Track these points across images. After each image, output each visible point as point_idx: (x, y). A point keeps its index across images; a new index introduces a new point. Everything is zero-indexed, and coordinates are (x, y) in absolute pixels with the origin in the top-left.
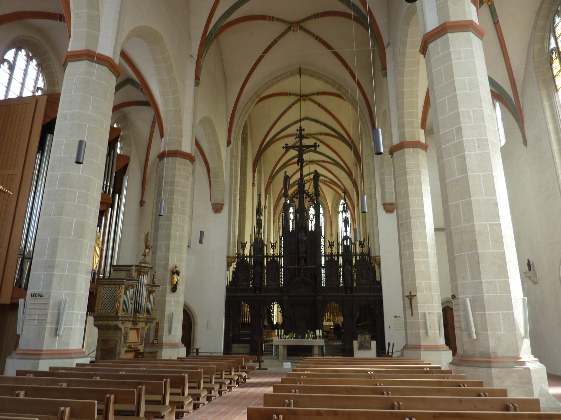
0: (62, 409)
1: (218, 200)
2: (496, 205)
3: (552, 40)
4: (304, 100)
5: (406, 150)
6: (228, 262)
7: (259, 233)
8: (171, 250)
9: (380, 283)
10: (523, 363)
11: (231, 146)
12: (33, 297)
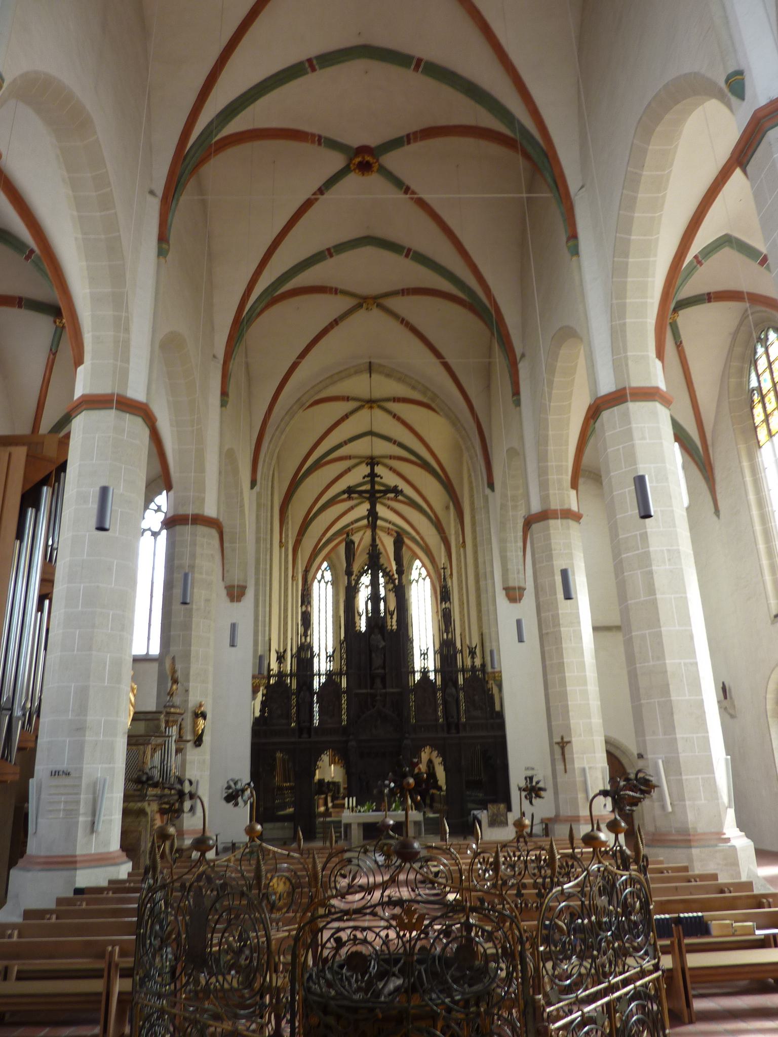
0: (110, 948)
1: (236, 578)
2: (691, 637)
3: (753, 376)
5: (552, 522)
6: (255, 685)
7: (305, 634)
8: (192, 678)
10: (728, 840)
11: (257, 488)
12: (55, 775)
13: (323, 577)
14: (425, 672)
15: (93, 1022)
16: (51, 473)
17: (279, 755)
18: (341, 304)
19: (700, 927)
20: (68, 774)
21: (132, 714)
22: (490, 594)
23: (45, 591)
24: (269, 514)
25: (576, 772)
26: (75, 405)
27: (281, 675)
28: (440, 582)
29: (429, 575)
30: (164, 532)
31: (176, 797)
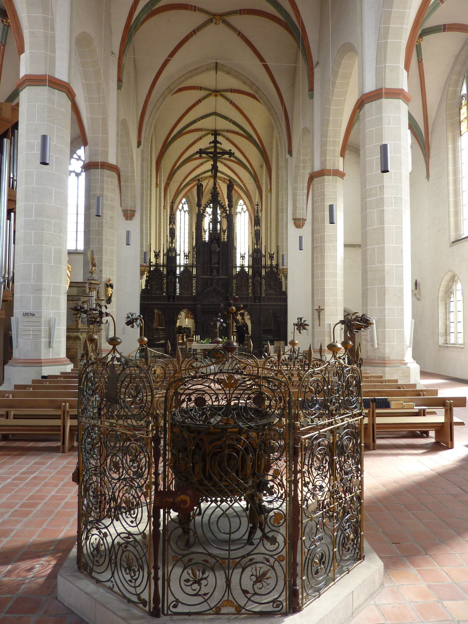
0: (64, 404)
4: (216, 96)
5: (326, 177)
7: (172, 242)
8: (103, 264)
9: (285, 294)
11: (141, 147)
13: (183, 207)
14: (242, 267)
15: (58, 440)
16: (9, 129)
17: (156, 311)
18: (199, 18)
19: (385, 404)
20: (34, 315)
21: (69, 282)
22: (284, 222)
23: (11, 207)
24: (149, 165)
25: (326, 326)
26: (21, 82)
27: (157, 265)
28: (254, 213)
29: (248, 209)
30: (83, 174)
31: (98, 315)
